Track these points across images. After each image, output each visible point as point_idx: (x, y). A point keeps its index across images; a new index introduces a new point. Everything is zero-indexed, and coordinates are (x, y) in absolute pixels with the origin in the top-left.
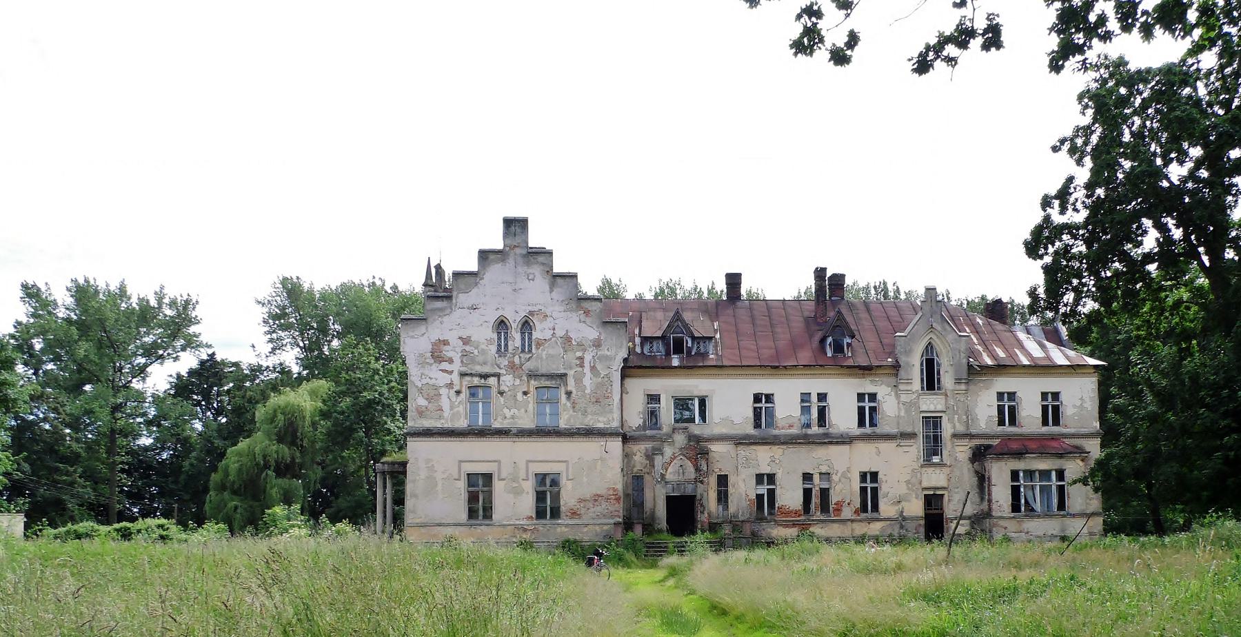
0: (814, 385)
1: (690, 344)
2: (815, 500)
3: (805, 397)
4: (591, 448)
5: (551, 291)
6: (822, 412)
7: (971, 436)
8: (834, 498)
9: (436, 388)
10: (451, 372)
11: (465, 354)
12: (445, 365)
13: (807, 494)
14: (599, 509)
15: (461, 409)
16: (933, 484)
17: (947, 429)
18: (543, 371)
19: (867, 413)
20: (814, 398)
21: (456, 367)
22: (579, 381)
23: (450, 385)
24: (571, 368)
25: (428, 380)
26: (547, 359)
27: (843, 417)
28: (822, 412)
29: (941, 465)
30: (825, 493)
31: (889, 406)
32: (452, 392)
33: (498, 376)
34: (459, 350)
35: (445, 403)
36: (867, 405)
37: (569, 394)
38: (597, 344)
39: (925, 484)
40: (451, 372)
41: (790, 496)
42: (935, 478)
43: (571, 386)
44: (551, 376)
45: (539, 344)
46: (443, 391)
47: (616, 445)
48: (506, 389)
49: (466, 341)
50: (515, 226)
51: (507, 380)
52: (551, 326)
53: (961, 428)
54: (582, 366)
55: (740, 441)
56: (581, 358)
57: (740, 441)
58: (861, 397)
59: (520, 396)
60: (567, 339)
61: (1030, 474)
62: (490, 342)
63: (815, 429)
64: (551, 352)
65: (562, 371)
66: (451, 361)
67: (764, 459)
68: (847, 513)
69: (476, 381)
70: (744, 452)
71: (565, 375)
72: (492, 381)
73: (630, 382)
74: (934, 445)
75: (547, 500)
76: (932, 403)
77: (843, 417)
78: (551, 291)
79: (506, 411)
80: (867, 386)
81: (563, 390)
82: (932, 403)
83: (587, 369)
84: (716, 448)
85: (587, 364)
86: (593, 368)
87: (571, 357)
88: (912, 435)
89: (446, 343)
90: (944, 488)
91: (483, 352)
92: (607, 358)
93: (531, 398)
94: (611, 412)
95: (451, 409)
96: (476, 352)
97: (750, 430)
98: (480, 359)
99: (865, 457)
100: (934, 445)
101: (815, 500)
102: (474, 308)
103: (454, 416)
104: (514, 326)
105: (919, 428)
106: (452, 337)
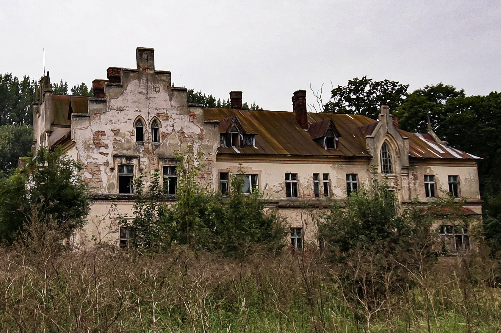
0: (322, 168)
3: (316, 176)
9: (97, 165)
11: (116, 142)
12: (103, 150)
20: (321, 177)
23: (106, 164)
32: (108, 170)
35: (104, 177)
36: (352, 182)
38: (201, 138)
40: (107, 155)
45: (165, 136)
46: (102, 168)
48: (144, 167)
50: (145, 55)
52: (171, 123)
63: (322, 198)
64: (172, 142)
66: (106, 146)
87: (184, 145)
89: (103, 133)
92: (208, 147)
96: (123, 141)
97: (283, 196)
98: (126, 145)
102: (121, 110)
104: (147, 123)
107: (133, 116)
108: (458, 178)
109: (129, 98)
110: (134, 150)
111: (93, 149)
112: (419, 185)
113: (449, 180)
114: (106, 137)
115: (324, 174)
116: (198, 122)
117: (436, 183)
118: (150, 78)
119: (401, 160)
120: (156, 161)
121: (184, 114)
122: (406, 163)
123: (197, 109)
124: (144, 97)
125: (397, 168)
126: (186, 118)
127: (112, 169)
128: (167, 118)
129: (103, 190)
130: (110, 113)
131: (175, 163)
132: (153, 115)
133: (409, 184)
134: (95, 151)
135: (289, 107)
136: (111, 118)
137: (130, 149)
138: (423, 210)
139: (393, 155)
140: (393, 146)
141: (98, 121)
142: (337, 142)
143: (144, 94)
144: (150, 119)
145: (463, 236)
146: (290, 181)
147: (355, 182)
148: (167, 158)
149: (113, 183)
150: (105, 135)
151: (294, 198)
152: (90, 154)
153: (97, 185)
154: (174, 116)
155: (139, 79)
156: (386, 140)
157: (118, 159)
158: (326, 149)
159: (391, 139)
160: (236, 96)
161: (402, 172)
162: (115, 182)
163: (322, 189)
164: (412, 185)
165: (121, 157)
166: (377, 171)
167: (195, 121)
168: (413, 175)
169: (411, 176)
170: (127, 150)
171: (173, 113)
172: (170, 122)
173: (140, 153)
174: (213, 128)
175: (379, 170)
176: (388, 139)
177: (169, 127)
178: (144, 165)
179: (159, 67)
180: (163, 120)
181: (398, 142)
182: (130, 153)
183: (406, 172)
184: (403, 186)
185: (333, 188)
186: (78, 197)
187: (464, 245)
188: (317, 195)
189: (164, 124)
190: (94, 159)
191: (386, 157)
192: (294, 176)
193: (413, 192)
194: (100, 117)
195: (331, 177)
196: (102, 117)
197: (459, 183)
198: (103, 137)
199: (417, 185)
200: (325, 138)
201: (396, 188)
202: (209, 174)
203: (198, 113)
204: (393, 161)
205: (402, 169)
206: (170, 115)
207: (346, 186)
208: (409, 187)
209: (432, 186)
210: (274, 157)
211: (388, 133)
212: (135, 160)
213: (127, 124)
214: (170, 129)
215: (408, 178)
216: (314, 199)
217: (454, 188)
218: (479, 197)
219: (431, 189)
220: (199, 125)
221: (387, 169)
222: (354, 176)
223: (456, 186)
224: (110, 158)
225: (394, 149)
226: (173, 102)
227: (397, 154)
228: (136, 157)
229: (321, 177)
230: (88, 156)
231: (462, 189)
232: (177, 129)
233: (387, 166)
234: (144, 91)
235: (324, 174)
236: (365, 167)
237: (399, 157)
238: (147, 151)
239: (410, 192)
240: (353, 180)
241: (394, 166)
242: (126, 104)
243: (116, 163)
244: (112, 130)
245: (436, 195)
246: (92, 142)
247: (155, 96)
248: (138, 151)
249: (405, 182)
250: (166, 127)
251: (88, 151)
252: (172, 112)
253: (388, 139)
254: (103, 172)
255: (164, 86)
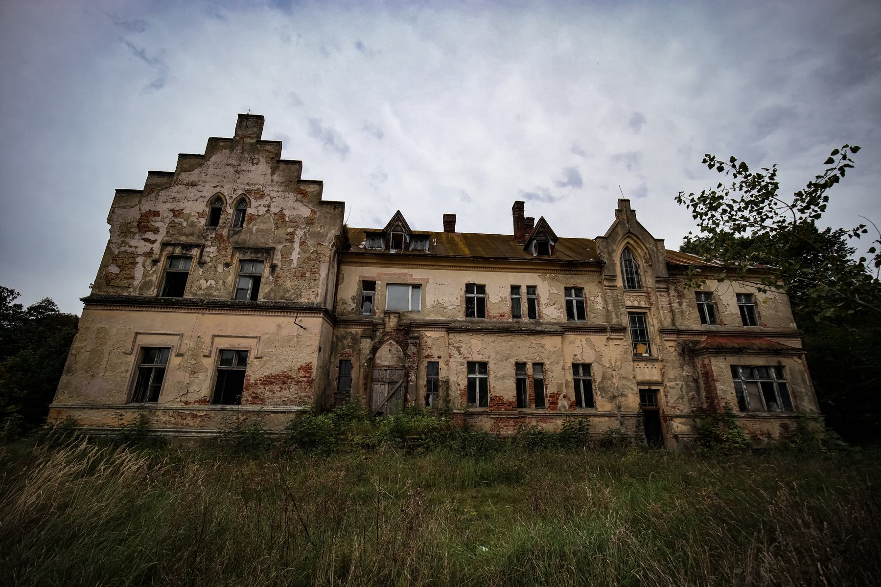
0: (525, 279)
1: (408, 241)
2: (529, 392)
3: (515, 289)
4: (286, 323)
5: (273, 173)
6: (532, 304)
7: (679, 332)
8: (550, 389)
9: (134, 256)
10: (153, 242)
11: (172, 225)
12: (150, 235)
13: (520, 384)
14: (286, 393)
15: (154, 278)
16: (647, 378)
17: (653, 324)
18: (250, 244)
19: (576, 309)
20: (524, 290)
21: (160, 237)
22: (286, 256)
23: (150, 254)
24: (280, 243)
25: (127, 248)
26: (255, 233)
27: (552, 312)
28: (532, 304)
29: (651, 360)
30: (539, 385)
31: (596, 298)
32: (149, 261)
33: (202, 247)
34: (168, 221)
35: (139, 272)
36: (574, 300)
37: (273, 267)
38: (309, 222)
39: (640, 378)
40: (153, 242)
41: (503, 386)
42: (650, 373)
43: (277, 259)
44: (256, 250)
45: (252, 218)
46: (140, 260)
47: (315, 323)
48: (208, 260)
49: (177, 213)
50: (250, 123)
51: (211, 251)
52: (267, 203)
53: (667, 323)
54: (292, 241)
55: (449, 328)
56: (292, 234)
57: (449, 328)
58: (568, 290)
59: (220, 269)
60: (281, 215)
61: (750, 369)
62: (200, 215)
63: (525, 319)
64: (262, 227)
65: (271, 245)
66: (156, 231)
67: (478, 347)
68: (563, 403)
69: (178, 251)
70: (455, 338)
71: (273, 249)
72: (195, 252)
73: (346, 269)
74: (640, 336)
75: (230, 381)
76: (632, 300)
77: (552, 312)
78: (273, 173)
79: (203, 282)
80: (576, 281)
81: (267, 265)
82: (632, 300)
83: (296, 246)
84: (430, 335)
85: (297, 240)
86: (302, 243)
87: (281, 233)
88: (623, 330)
89: (156, 214)
90: (656, 383)
91: (192, 225)
92: (319, 235)
93: (232, 270)
94: (317, 286)
95: (144, 276)
96: (185, 224)
97: (461, 317)
98: (187, 230)
99: (580, 347)
100: (640, 336)
101: (529, 392)
102: (193, 185)
103: (146, 285)
104: (229, 201)
105: (625, 321)
106: (164, 208)
107: (209, 191)
108: (753, 298)
109: (211, 171)
110: (199, 237)
111: (135, 234)
112: (688, 306)
113: (739, 300)
114: (160, 219)
115: (528, 287)
116: (309, 202)
117: (716, 303)
118: (247, 147)
119: (654, 270)
120: (230, 251)
121: (290, 191)
122: (664, 273)
123: (312, 186)
124: (232, 170)
125: (648, 281)
126: (292, 197)
127: (155, 262)
128: (262, 196)
129: (131, 290)
130: (176, 188)
131: (259, 255)
132: (240, 192)
133: (670, 303)
134: (137, 236)
135: (507, 228)
136: (174, 195)
137: (192, 234)
138: (698, 342)
139: (641, 263)
140: (639, 251)
141: (153, 198)
142: (553, 247)
143: (234, 166)
144: (235, 196)
145: (775, 385)
146: (475, 295)
147: (580, 299)
148: (249, 248)
149: (150, 281)
150: (159, 216)
151: (476, 319)
152: (128, 240)
153: (124, 283)
154: (273, 194)
155: (232, 149)
156: (628, 243)
157: (170, 248)
158: (535, 255)
159: (635, 241)
160: (449, 221)
161: (657, 286)
162: (154, 278)
163: (524, 306)
164: (675, 305)
165: (175, 245)
166: (615, 284)
167: (305, 200)
168: (675, 291)
169: (672, 293)
170: (187, 236)
171: (274, 191)
172: (265, 201)
173: (207, 240)
174: (332, 210)
175: (619, 283)
176: (632, 242)
177: (261, 208)
178: (208, 256)
179: (267, 135)
180: (255, 198)
181: (647, 245)
182: (191, 240)
183: (663, 286)
184: (660, 306)
185: (542, 307)
186: (700, 409)
187: (779, 400)
188: (516, 315)
189: (254, 203)
190: (131, 247)
191: (631, 266)
192: (481, 288)
193: (678, 316)
194: (158, 193)
195: (539, 291)
196: (162, 193)
197: (756, 305)
198: (156, 218)
199: (684, 306)
200: (535, 242)
201: (649, 309)
202: (314, 273)
203: (312, 190)
204: (641, 272)
205: (657, 282)
206: (266, 192)
207: (564, 304)
208: (671, 307)
209: (711, 308)
210: (447, 262)
211: (629, 232)
212: (196, 249)
213: (197, 203)
214: (263, 210)
215: (669, 295)
216: (510, 320)
217: (748, 311)
218: (793, 325)
219: (708, 310)
220: (310, 206)
221: (632, 283)
222: (579, 291)
223: (751, 310)
224: (157, 247)
225: (642, 254)
226: (275, 177)
227: (647, 262)
228: (197, 246)
229: (524, 290)
230: (123, 242)
231: (763, 313)
232: (274, 210)
233: (632, 280)
234: (234, 163)
235: (528, 287)
236: (596, 278)
237: (650, 266)
238: (219, 238)
239: (674, 315)
240: (576, 295)
241: (643, 278)
242: (203, 178)
243: (164, 253)
244: (172, 210)
245: (718, 321)
246: (135, 224)
247: (250, 168)
248: (205, 238)
249: (663, 301)
250: (256, 207)
251: (125, 236)
252: (271, 188)
253: (632, 242)
254: (140, 265)
255: (267, 157)
